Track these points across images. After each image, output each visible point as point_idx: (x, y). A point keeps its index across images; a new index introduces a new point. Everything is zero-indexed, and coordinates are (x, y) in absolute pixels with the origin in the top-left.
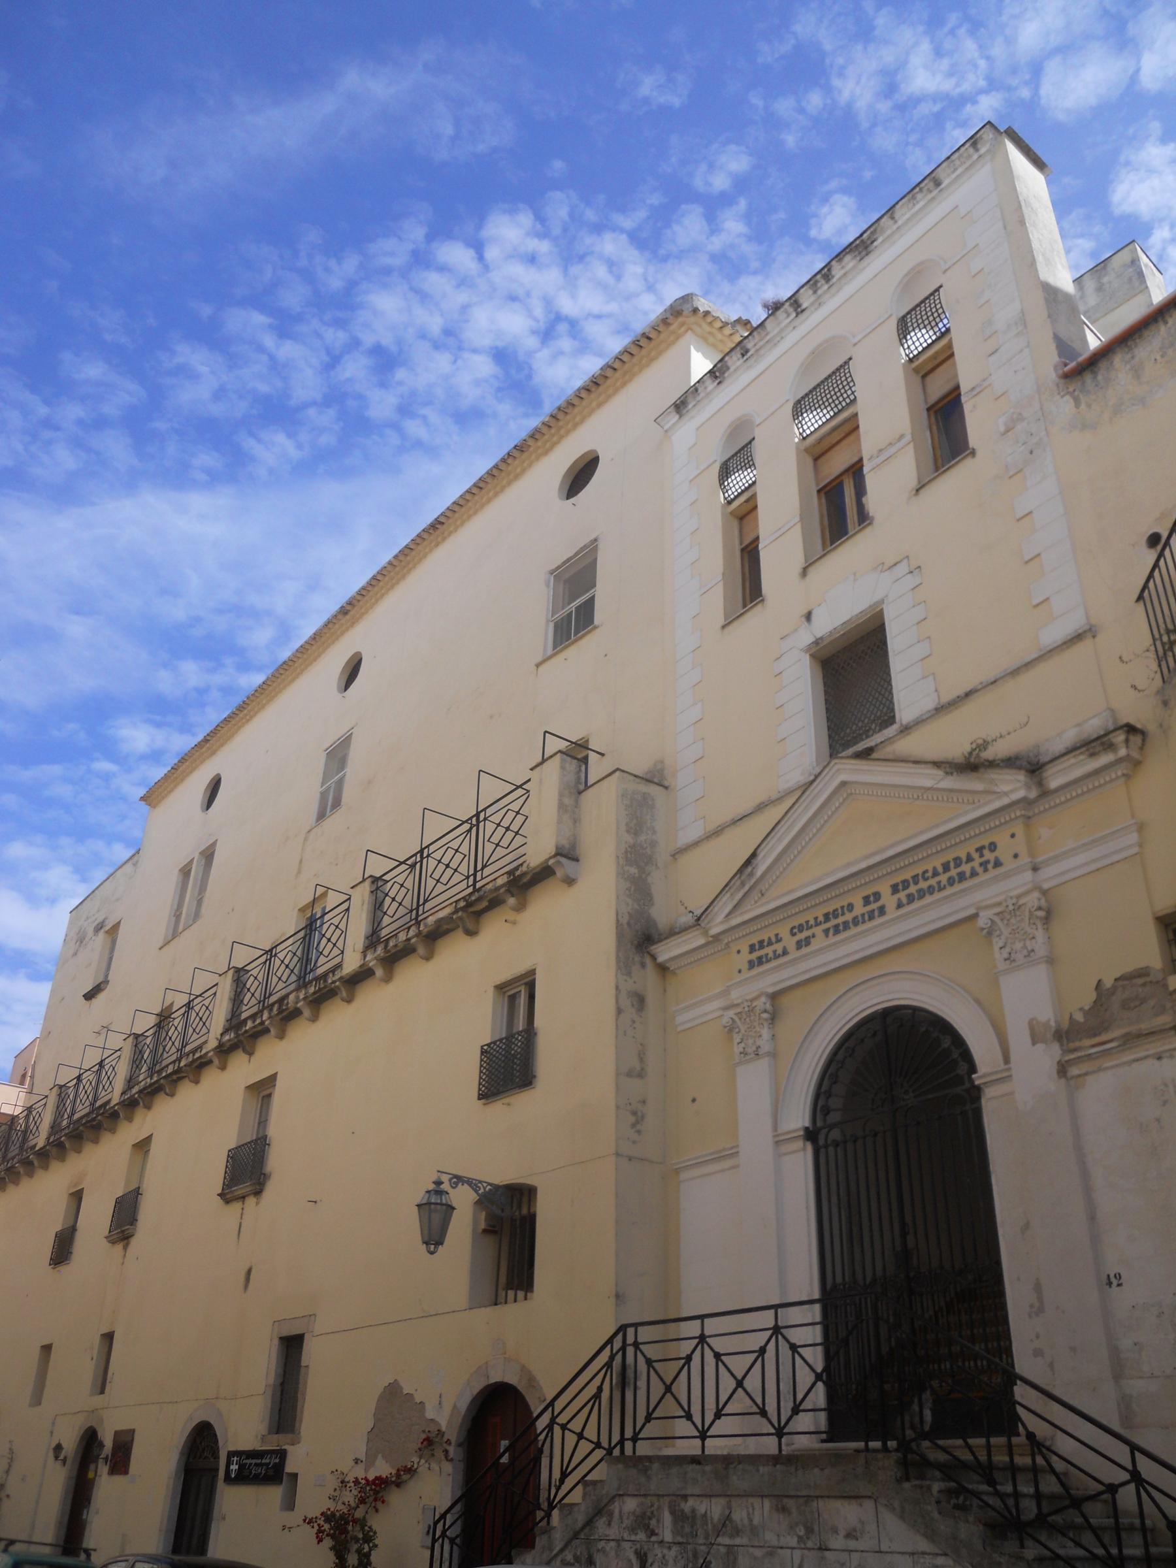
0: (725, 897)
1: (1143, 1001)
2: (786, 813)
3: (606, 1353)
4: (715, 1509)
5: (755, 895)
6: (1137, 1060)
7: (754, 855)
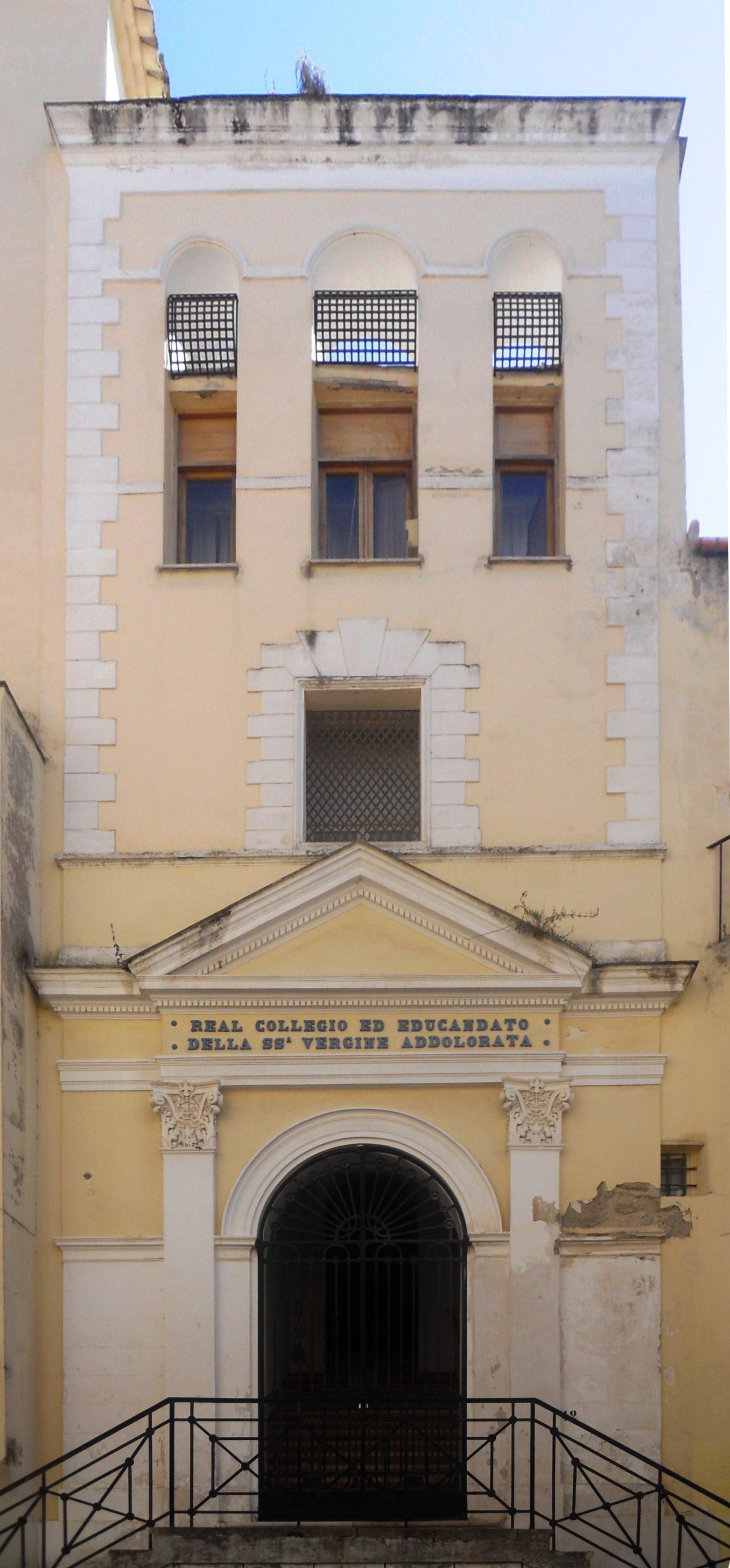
1: (636, 1210)
2: (283, 879)
3: (141, 1426)
5: (211, 963)
6: (622, 1255)
7: (226, 913)
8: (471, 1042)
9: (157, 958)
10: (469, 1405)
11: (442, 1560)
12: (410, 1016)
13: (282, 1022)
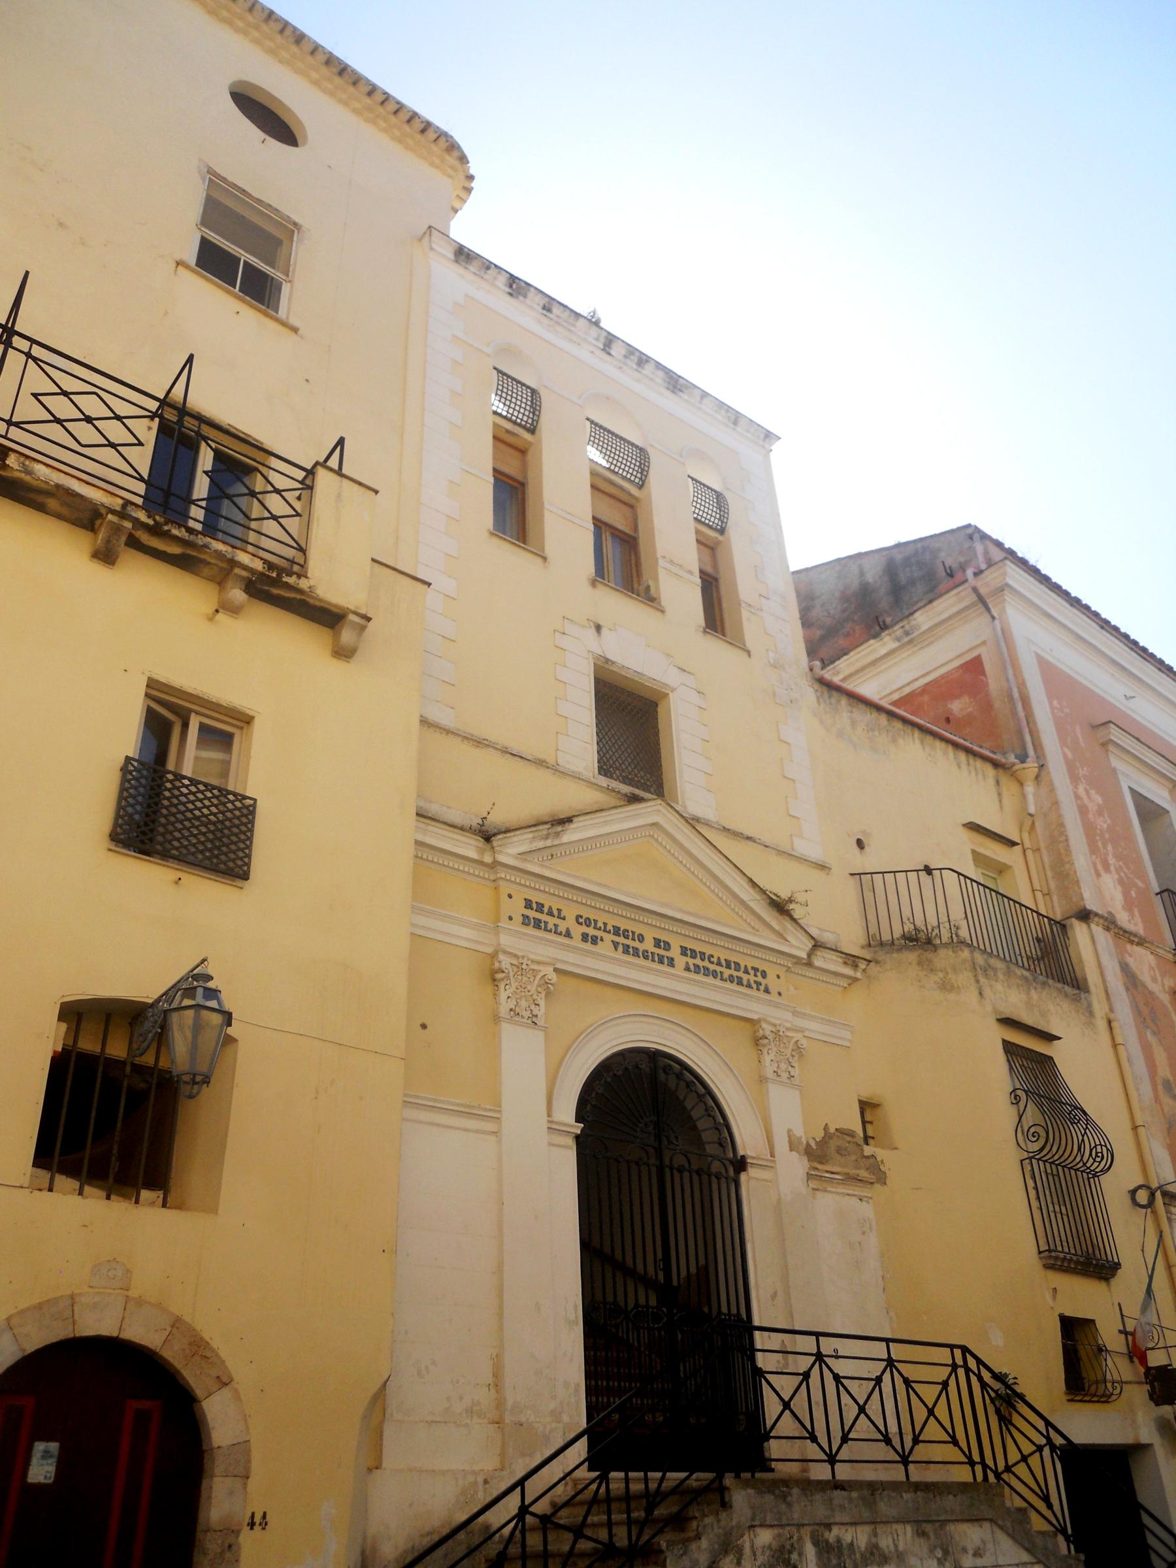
0: (527, 835)
4: (860, 1537)
8: (731, 979)
9: (515, 839)
10: (757, 1334)
11: (943, 1518)
12: (690, 945)
13: (596, 921)
